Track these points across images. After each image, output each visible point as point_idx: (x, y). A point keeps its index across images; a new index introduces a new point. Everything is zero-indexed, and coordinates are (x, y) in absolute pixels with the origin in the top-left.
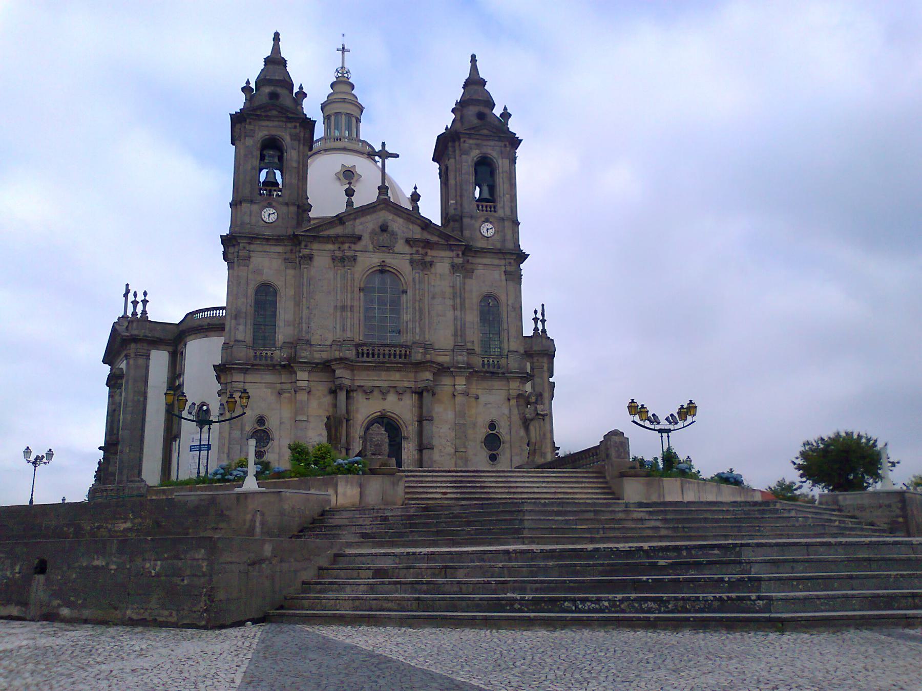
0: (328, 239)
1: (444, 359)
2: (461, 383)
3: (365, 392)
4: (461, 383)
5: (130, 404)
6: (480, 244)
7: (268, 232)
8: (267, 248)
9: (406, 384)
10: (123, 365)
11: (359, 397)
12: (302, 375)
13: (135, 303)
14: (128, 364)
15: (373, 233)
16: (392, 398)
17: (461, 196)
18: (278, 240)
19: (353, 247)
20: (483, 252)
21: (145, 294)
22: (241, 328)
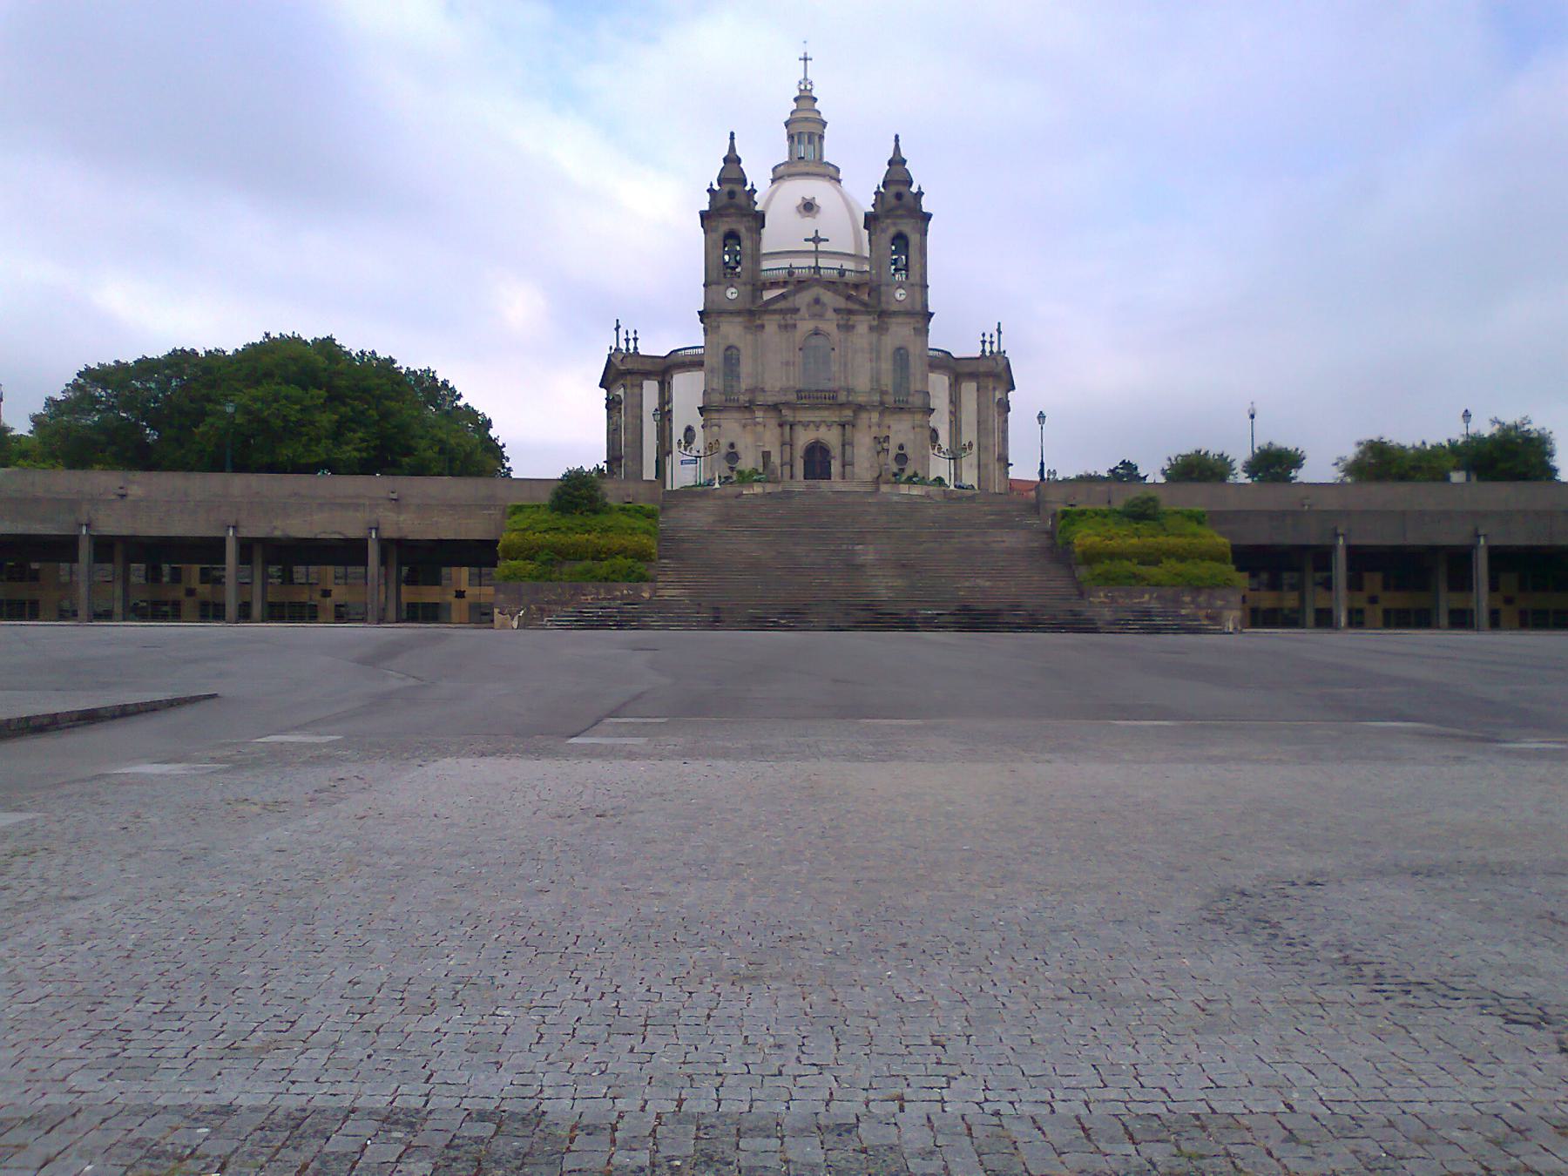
0: (775, 312)
1: (861, 399)
2: (875, 416)
3: (803, 425)
4: (875, 416)
5: (630, 426)
6: (894, 307)
7: (731, 308)
8: (731, 319)
9: (834, 419)
10: (621, 392)
11: (799, 430)
12: (759, 414)
13: (627, 340)
14: (625, 393)
15: (809, 305)
16: (823, 429)
17: (880, 267)
18: (739, 313)
19: (794, 316)
20: (895, 314)
21: (635, 332)
22: (716, 380)
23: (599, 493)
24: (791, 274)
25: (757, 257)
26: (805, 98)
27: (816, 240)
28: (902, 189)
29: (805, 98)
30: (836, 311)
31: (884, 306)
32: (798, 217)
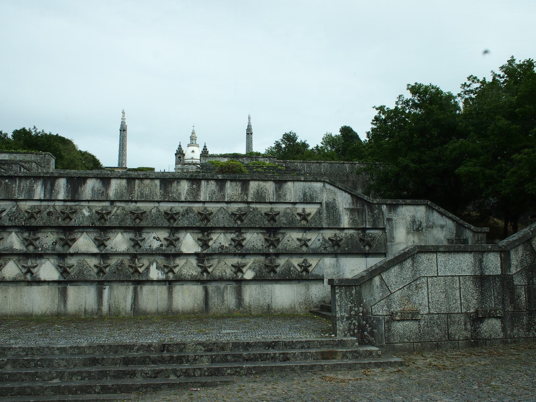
25: (184, 160)
28: (206, 151)
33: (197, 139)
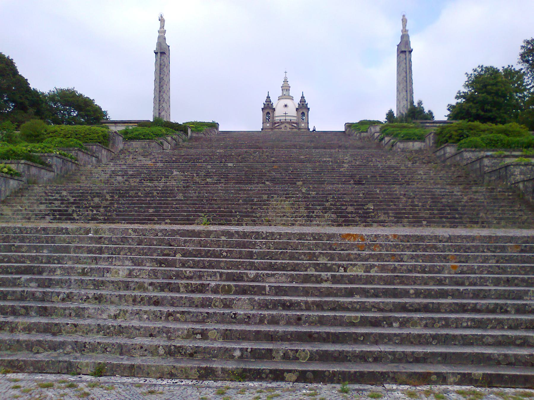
6: (302, 127)
23: (376, 353)
24: (280, 121)
26: (286, 81)
27: (286, 114)
29: (286, 81)
30: (290, 128)
31: (300, 127)
32: (283, 108)
33: (291, 89)
